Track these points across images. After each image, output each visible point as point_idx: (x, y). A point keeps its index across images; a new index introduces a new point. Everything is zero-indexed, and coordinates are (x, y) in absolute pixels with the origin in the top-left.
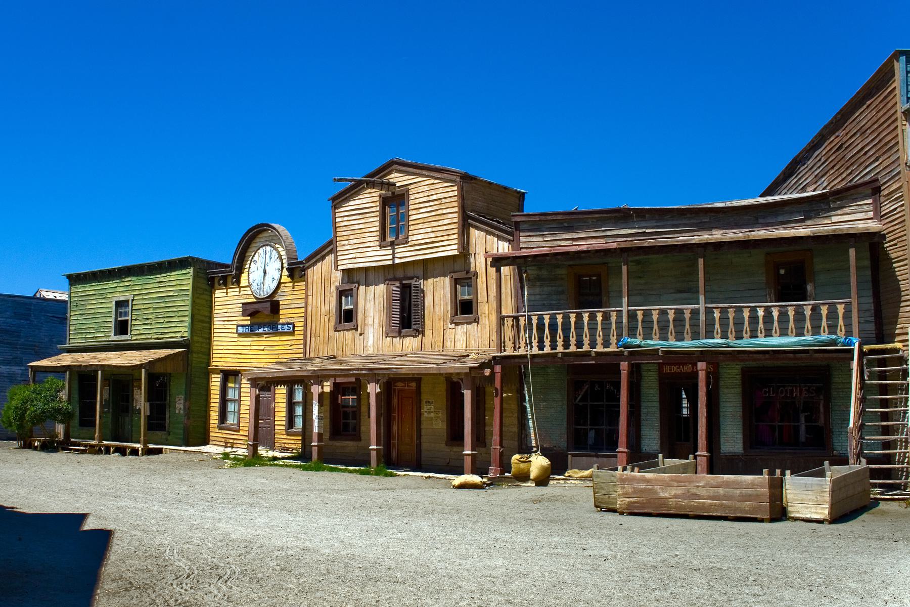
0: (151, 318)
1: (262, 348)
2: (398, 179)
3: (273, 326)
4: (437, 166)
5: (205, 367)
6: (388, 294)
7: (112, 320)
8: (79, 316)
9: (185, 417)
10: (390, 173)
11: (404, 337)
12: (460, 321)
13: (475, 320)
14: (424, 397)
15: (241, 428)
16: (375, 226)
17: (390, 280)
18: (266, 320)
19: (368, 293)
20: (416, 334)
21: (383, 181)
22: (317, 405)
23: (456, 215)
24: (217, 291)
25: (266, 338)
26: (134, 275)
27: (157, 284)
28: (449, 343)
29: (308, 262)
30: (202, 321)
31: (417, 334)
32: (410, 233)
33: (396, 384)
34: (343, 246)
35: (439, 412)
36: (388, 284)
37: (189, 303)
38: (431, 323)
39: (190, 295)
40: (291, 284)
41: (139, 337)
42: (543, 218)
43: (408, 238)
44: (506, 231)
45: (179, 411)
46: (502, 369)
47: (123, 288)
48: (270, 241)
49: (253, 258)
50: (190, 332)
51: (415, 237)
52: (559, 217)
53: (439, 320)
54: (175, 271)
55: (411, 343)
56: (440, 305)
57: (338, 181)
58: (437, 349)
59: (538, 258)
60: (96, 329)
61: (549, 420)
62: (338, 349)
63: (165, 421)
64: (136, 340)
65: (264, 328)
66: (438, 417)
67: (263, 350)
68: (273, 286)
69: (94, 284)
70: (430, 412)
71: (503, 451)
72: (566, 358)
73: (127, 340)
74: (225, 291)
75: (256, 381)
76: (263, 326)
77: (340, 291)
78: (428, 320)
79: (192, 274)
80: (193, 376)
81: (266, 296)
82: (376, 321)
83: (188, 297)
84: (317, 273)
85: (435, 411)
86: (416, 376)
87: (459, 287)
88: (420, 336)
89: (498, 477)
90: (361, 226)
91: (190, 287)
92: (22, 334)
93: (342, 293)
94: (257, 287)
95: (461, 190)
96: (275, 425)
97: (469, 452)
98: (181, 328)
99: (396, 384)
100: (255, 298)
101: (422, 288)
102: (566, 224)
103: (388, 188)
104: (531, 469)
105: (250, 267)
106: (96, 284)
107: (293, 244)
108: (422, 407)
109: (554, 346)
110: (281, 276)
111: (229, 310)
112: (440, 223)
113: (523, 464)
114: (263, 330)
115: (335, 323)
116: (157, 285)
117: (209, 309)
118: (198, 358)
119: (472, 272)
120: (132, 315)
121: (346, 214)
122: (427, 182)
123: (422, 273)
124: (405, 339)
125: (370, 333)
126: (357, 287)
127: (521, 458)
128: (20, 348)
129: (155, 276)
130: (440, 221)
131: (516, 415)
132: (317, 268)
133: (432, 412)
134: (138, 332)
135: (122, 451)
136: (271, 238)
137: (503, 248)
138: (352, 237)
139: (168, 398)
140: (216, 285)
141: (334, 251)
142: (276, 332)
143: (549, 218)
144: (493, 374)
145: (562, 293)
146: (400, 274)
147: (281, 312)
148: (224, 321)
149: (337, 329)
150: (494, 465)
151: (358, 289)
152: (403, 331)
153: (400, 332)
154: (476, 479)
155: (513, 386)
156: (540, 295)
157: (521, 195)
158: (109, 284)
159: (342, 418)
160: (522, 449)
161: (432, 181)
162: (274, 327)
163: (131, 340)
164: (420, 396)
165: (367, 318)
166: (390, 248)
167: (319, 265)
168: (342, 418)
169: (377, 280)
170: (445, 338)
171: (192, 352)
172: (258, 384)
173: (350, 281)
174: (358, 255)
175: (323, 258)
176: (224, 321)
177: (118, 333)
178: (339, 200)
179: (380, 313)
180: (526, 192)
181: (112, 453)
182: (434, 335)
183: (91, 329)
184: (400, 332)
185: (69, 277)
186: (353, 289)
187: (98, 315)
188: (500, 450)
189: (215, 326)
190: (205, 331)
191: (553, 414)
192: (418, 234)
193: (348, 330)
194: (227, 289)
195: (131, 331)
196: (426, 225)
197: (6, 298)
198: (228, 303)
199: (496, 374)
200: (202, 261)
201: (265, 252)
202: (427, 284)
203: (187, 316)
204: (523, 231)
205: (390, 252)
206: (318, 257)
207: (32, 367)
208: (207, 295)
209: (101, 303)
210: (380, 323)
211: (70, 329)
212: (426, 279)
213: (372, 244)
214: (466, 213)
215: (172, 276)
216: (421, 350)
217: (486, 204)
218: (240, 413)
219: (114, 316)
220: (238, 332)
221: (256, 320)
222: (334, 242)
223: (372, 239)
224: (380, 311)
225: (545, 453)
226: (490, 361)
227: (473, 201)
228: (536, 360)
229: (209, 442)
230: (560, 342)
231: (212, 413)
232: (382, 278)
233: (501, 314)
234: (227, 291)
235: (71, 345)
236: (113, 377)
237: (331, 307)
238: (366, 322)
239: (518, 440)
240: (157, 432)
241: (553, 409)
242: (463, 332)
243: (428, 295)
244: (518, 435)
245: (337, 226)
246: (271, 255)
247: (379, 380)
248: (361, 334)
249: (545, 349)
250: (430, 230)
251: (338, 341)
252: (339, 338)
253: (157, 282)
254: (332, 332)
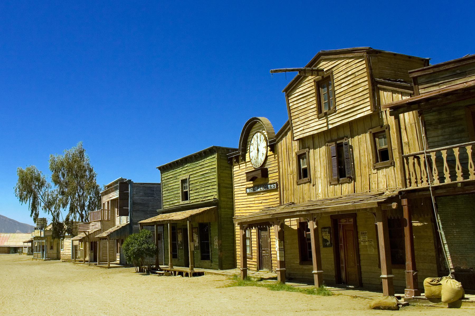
0: (198, 189)
1: (260, 202)
2: (325, 65)
3: (265, 186)
4: (349, 49)
5: (230, 218)
6: (329, 152)
7: (180, 192)
8: (166, 191)
9: (219, 250)
10: (319, 63)
11: (342, 184)
12: (380, 167)
13: (391, 164)
14: (360, 229)
15: (253, 257)
16: (314, 104)
17: (329, 142)
18: (262, 183)
19: (316, 154)
20: (349, 180)
21: (312, 69)
22: (278, 240)
23: (367, 83)
24: (234, 167)
25: (262, 194)
26: (189, 163)
27: (200, 166)
28: (374, 185)
29: (278, 138)
30: (226, 188)
31: (350, 181)
32: (337, 104)
33: (340, 221)
34: (296, 122)
35: (371, 241)
36: (327, 146)
37: (216, 176)
38: (360, 171)
39: (217, 171)
40: (273, 156)
41: (193, 201)
42: (436, 70)
43: (335, 108)
44: (407, 87)
45: (216, 247)
46: (409, 202)
47: (184, 171)
48: (260, 129)
49: (251, 142)
50: (218, 195)
51: (340, 107)
52: (451, 66)
53: (365, 168)
54: (208, 157)
55: (347, 188)
56: (365, 156)
57: (274, 72)
58: (365, 191)
59: (430, 101)
60: (174, 198)
61: (463, 245)
62: (301, 198)
63: (209, 253)
64: (192, 203)
65: (261, 188)
66: (371, 245)
67: (261, 203)
68: (263, 159)
69: (171, 171)
70: (365, 241)
71: (416, 274)
72: (466, 187)
73: (188, 204)
74: (238, 166)
75: (242, 225)
76: (260, 187)
77: (298, 155)
78: (357, 168)
79: (216, 157)
80: (222, 223)
81: (259, 166)
82: (322, 174)
83: (216, 172)
84: (284, 145)
85: (368, 241)
86: (340, 213)
87: (377, 139)
88: (353, 182)
89: (413, 298)
90: (305, 106)
91: (216, 166)
92: (150, 205)
93: (300, 157)
94: (254, 161)
95: (368, 63)
96: (271, 254)
97: (386, 276)
98: (213, 193)
99: (340, 221)
100: (255, 168)
101: (350, 144)
102: (458, 71)
103: (318, 74)
104: (442, 292)
105: (250, 149)
106: (172, 171)
107: (272, 128)
108: (359, 237)
109: (453, 176)
110: (267, 151)
111: (242, 179)
112: (357, 91)
113: (435, 286)
114: (260, 190)
115: (297, 179)
116: (200, 167)
117: (230, 179)
118: (225, 211)
119: (385, 125)
120: (189, 188)
121: (295, 99)
122: (344, 63)
123: (349, 133)
124: (343, 185)
125: (319, 184)
126: (308, 151)
127: (432, 281)
128: (149, 213)
129: (199, 162)
130: (357, 90)
131: (432, 241)
132: (283, 141)
133: (366, 241)
134: (194, 198)
135: (181, 273)
136: (260, 127)
137: (399, 98)
138: (300, 115)
139: (210, 239)
140: (234, 163)
141: (291, 129)
142: (267, 190)
143: (441, 68)
144: (400, 207)
145: (463, 131)
146: (335, 137)
147: (269, 176)
148: (239, 186)
149: (299, 183)
150: (409, 287)
151: (309, 152)
152: (341, 179)
153: (338, 181)
154: (392, 300)
155: (426, 216)
156: (442, 135)
157: (425, 62)
158: (178, 170)
159: (308, 249)
160: (440, 271)
161: (347, 61)
162: (266, 186)
163: (190, 203)
164: (357, 229)
165: (317, 172)
166: (324, 118)
167: (284, 139)
168: (308, 249)
169: (320, 144)
170: (370, 181)
171: (220, 208)
172: (244, 227)
173: (304, 147)
174: (306, 127)
175: (286, 134)
176: (239, 186)
177: (184, 199)
178: (290, 90)
179: (325, 168)
180: (430, 59)
181: (177, 275)
182: (362, 181)
183: (172, 198)
184: (338, 181)
185: (160, 168)
186: (306, 152)
187: (174, 189)
188: (413, 273)
189: (235, 190)
190: (229, 193)
191: (466, 239)
192: (342, 105)
193: (305, 183)
194: (239, 165)
195: (190, 197)
196: (346, 96)
197: (139, 185)
198: (240, 174)
199: (404, 207)
200: (223, 149)
201: (257, 137)
202: (354, 140)
203: (216, 185)
204: (421, 84)
205: (325, 121)
206: (283, 133)
207: (140, 223)
208: (228, 170)
209: (175, 182)
210: (325, 176)
211: (163, 200)
212: (352, 137)
213: (313, 117)
214: (375, 80)
215: (207, 161)
216: (354, 192)
217: (393, 72)
218: (252, 247)
219: (181, 190)
220: (247, 192)
221: (256, 183)
222: (290, 121)
223: (313, 113)
224: (324, 166)
225: (457, 277)
226: (397, 196)
227: (381, 70)
228: (439, 192)
229: (236, 266)
230: (459, 173)
231: (237, 247)
232: (323, 142)
233: (403, 154)
234: (239, 166)
235: (164, 209)
236: (183, 227)
237: (293, 168)
238: (316, 176)
239: (437, 263)
240: (206, 261)
241: (466, 234)
242: (383, 175)
243: (355, 149)
244: (436, 259)
245: (291, 109)
246: (260, 138)
247: (315, 219)
248: (313, 185)
249: (446, 181)
250: (350, 99)
251: (300, 191)
252: (300, 189)
253: (200, 165)
254: (295, 186)
